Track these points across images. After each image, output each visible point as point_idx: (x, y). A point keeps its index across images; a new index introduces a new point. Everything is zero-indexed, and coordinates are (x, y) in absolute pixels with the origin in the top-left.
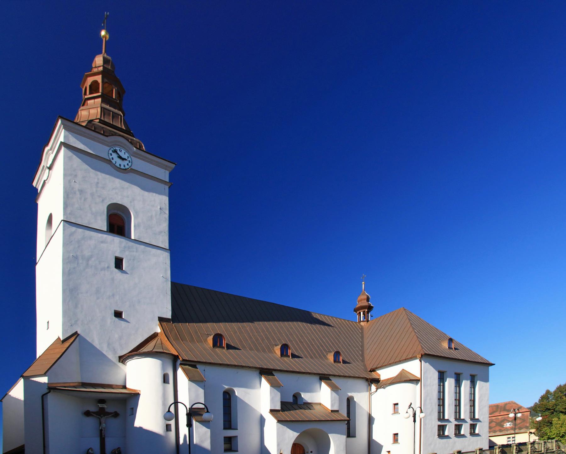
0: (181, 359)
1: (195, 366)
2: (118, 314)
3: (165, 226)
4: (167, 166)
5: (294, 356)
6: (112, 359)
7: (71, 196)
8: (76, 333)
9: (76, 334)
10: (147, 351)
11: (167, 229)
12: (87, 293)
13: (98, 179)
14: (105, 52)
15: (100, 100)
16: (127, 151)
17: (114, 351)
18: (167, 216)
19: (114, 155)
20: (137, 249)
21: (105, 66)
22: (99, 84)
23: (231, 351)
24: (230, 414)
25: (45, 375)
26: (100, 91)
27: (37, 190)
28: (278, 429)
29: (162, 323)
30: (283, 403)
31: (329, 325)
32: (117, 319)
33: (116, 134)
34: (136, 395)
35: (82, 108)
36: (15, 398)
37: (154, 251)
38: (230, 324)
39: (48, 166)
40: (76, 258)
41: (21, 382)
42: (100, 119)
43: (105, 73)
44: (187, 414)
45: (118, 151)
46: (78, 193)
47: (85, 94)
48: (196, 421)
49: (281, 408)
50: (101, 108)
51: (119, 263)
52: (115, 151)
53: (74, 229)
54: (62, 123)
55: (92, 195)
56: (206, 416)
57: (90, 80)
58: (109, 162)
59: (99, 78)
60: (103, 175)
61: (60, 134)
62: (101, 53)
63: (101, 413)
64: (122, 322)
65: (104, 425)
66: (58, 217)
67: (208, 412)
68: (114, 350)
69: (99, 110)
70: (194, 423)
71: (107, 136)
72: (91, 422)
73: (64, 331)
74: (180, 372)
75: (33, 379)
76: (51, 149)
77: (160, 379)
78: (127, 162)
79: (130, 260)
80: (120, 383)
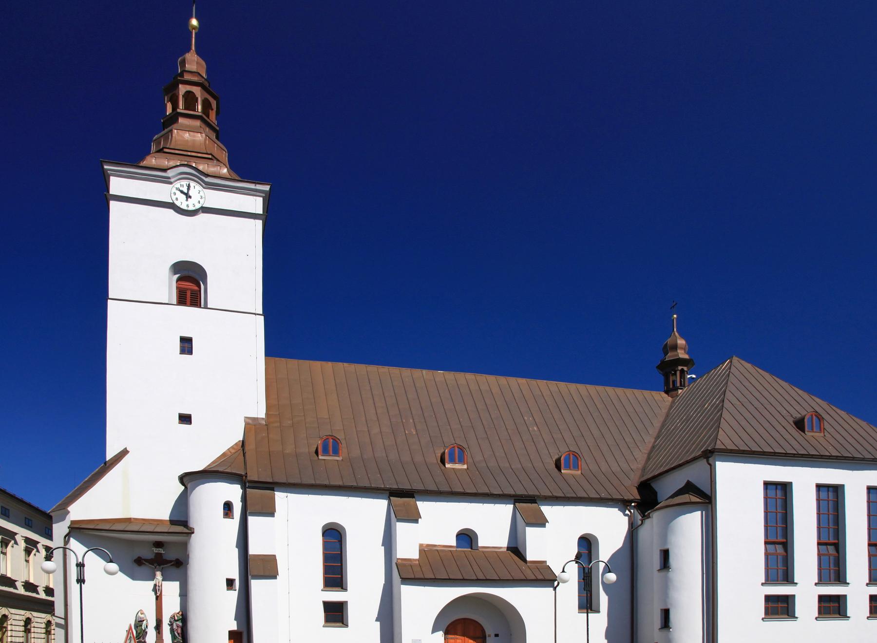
5: (27, 561)
51: (187, 345)
58: (171, 206)
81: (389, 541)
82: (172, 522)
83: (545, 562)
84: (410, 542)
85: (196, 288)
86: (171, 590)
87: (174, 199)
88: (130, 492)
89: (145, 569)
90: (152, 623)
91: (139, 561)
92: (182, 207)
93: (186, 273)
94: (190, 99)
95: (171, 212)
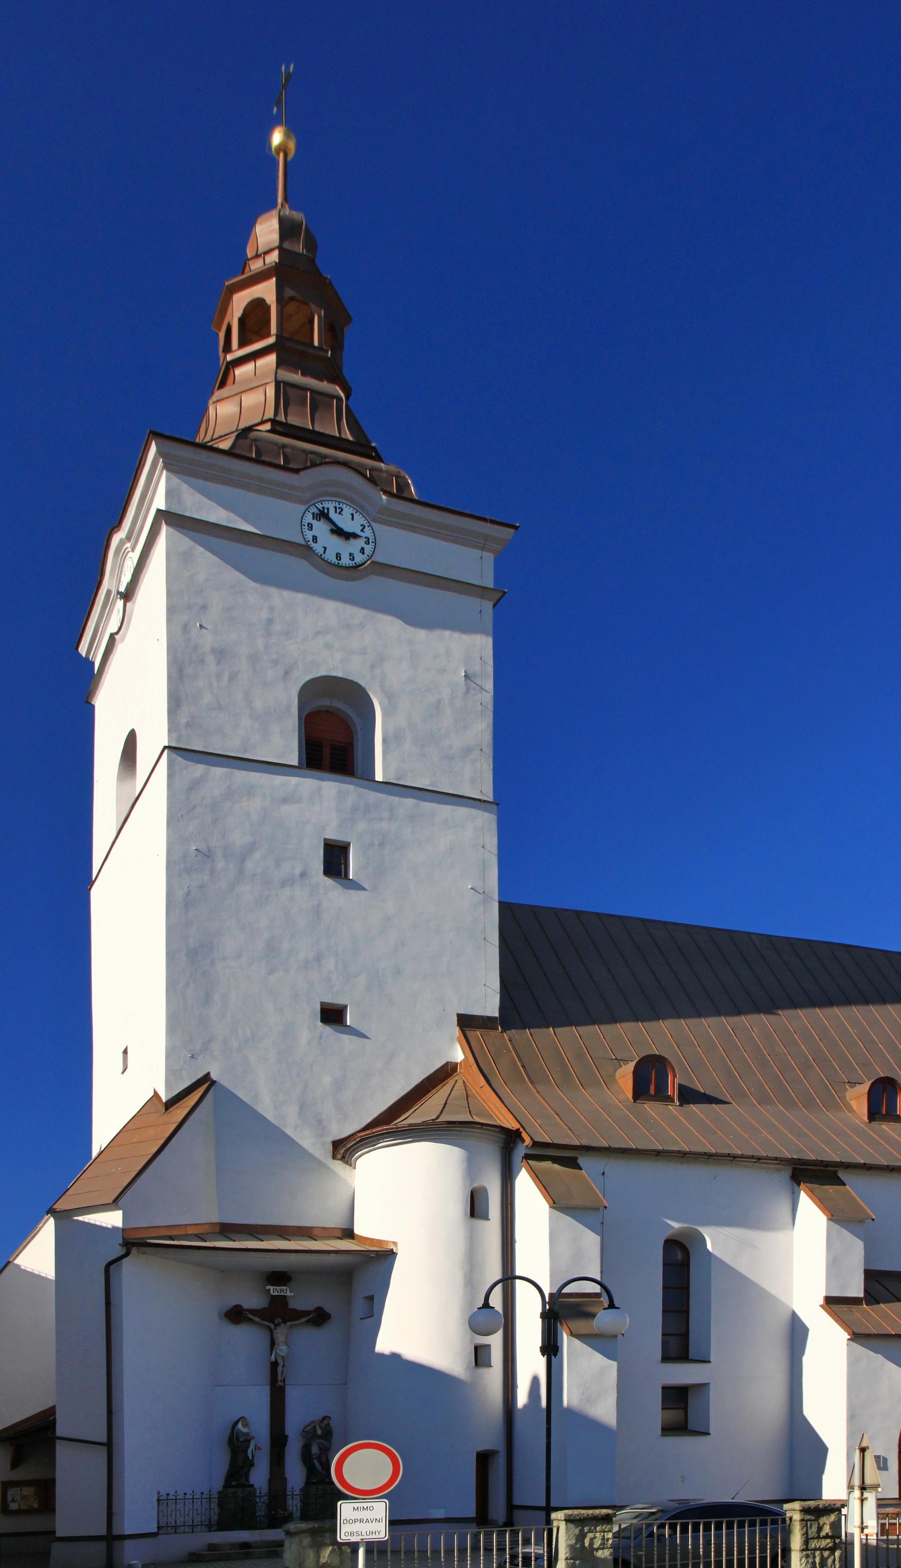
0: (528, 1141)
1: (572, 1163)
2: (332, 1015)
3: (481, 729)
4: (486, 538)
6: (311, 1150)
7: (189, 671)
8: (206, 1077)
9: (206, 1081)
10: (419, 1120)
11: (487, 738)
12: (239, 956)
13: (271, 609)
14: (286, 199)
15: (272, 359)
16: (360, 508)
17: (320, 1125)
18: (488, 697)
19: (321, 528)
20: (391, 811)
21: (286, 245)
22: (268, 308)
23: (694, 1108)
24: (687, 1288)
25: (114, 1204)
26: (274, 329)
27: (92, 664)
28: (853, 1362)
29: (470, 1034)
30: (871, 1276)
32: (328, 1030)
33: (324, 461)
34: (381, 1258)
35: (218, 394)
36: (31, 1274)
37: (445, 811)
38: (692, 1022)
39: (122, 589)
40: (206, 855)
41: (48, 1230)
42: (273, 421)
43: (285, 272)
44: (544, 1315)
45: (332, 515)
46: (211, 659)
47: (228, 348)
48: (572, 1334)
49: (866, 1291)
50: (278, 383)
51: (335, 859)
52: (323, 515)
53: (199, 769)
54: (159, 453)
55: (254, 659)
56: (604, 1320)
57: (240, 301)
58: (304, 550)
59: (267, 291)
60: (286, 593)
61: (157, 488)
62: (273, 205)
63: (276, 1314)
64: (346, 1038)
65: (284, 1348)
66: (154, 740)
67: (612, 1306)
68: (320, 1122)
69: (271, 391)
70: (566, 1341)
71: (296, 471)
72: (247, 1339)
73: (171, 1074)
74: (525, 1184)
75: (80, 1218)
76: (128, 538)
77: (457, 1206)
78: (360, 543)
79: (371, 845)
80: (335, 1221)
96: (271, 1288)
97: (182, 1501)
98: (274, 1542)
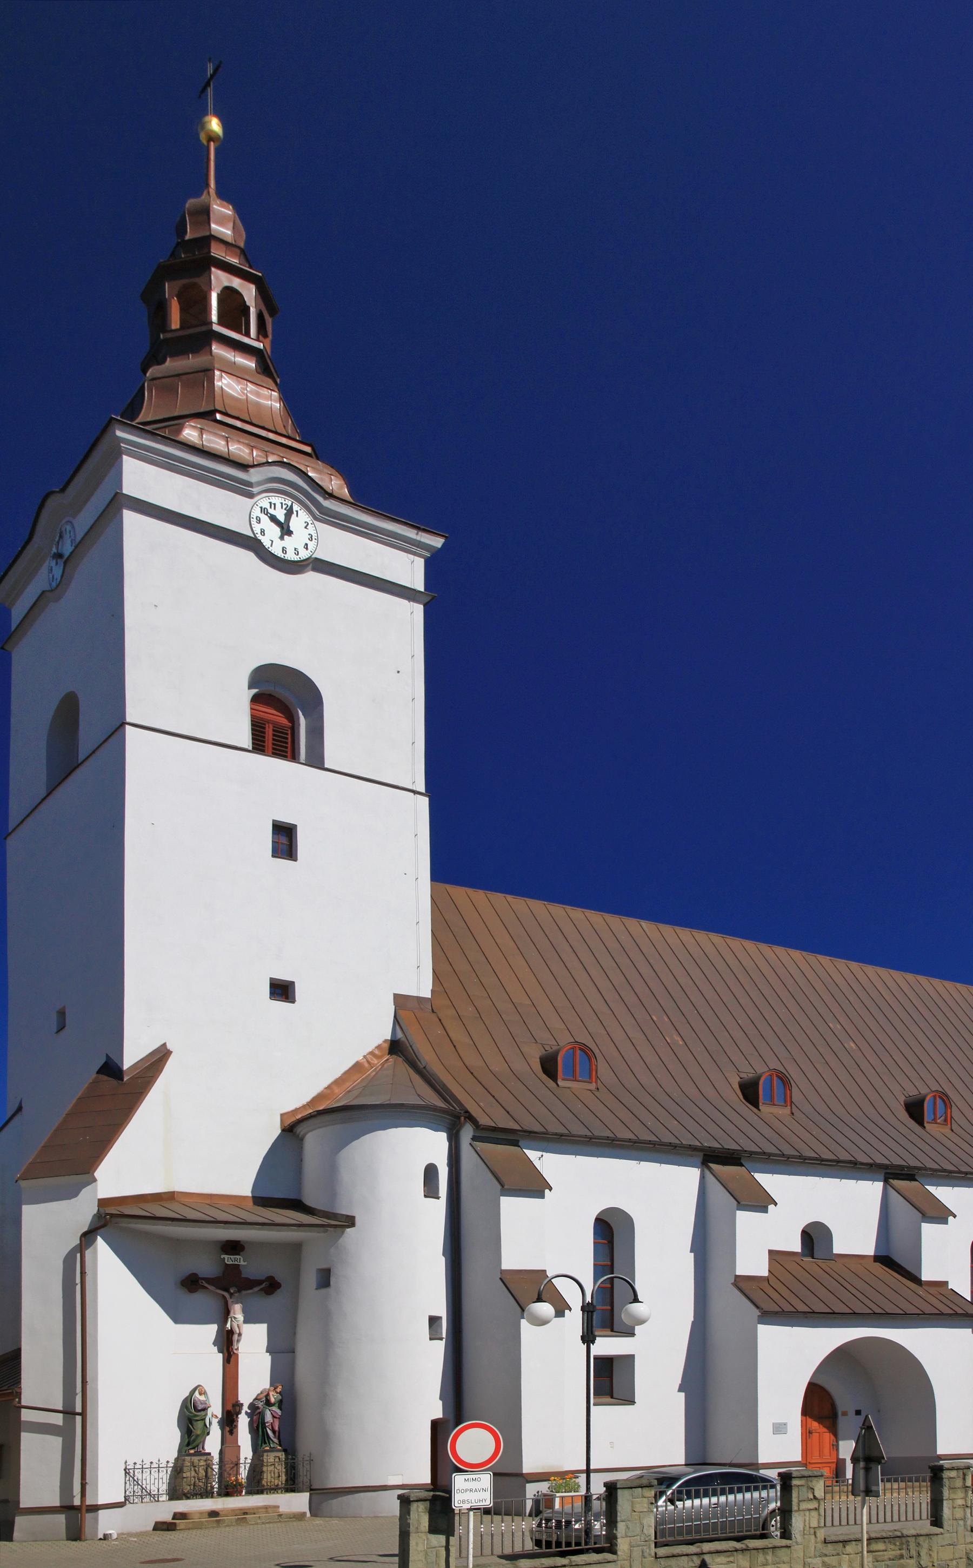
31: (178, 1560)
51: (285, 840)
58: (252, 544)
81: (702, 1245)
82: (260, 1200)
83: (946, 1283)
84: (757, 1241)
85: (284, 721)
86: (254, 1340)
87: (257, 530)
88: (192, 1141)
89: (204, 1300)
90: (216, 1409)
91: (192, 1283)
92: (273, 550)
93: (269, 689)
94: (234, 309)
95: (249, 557)
96: (226, 1257)
97: (148, 1470)
98: (241, 1509)
